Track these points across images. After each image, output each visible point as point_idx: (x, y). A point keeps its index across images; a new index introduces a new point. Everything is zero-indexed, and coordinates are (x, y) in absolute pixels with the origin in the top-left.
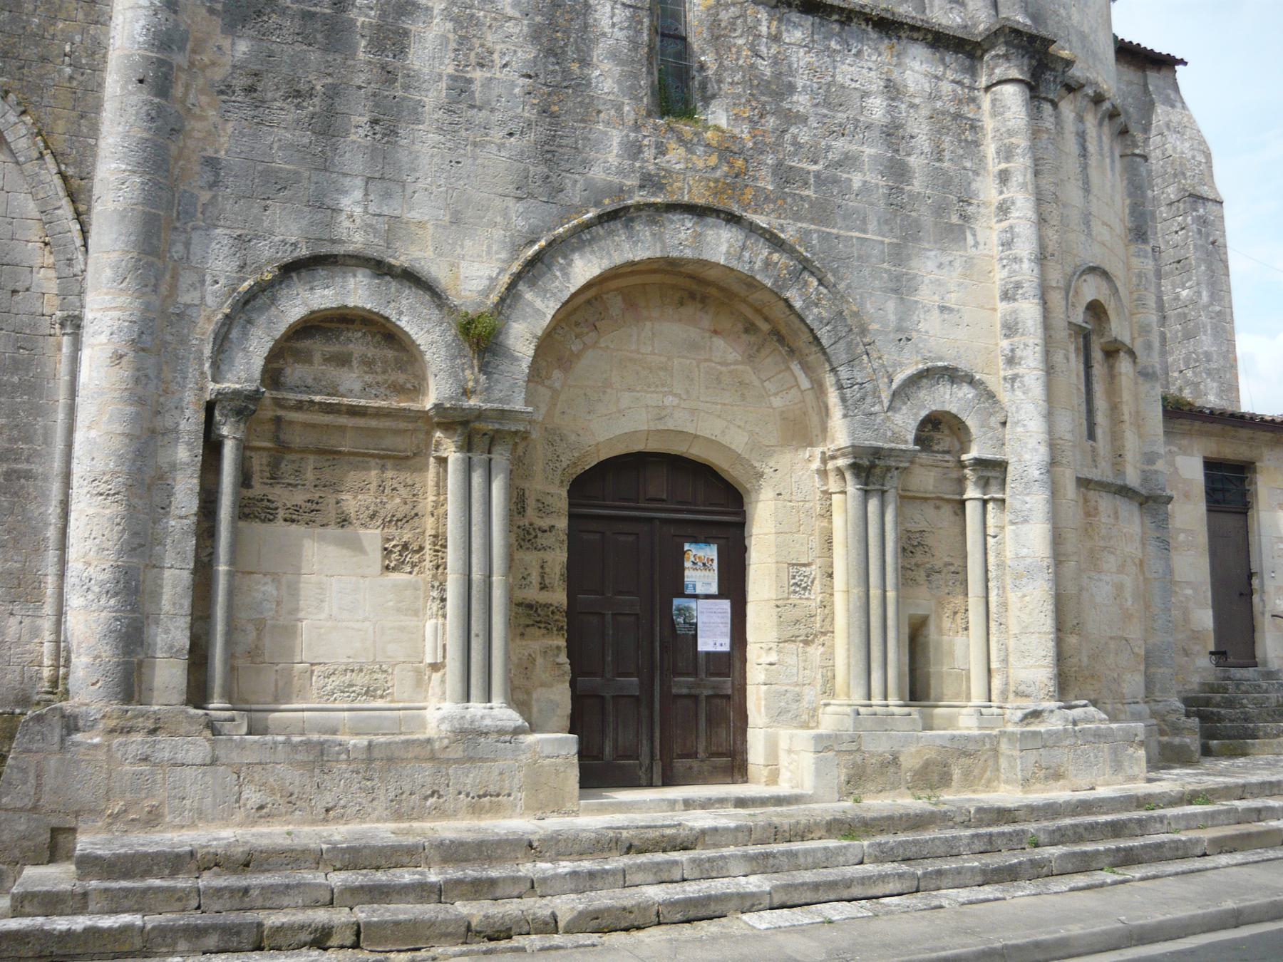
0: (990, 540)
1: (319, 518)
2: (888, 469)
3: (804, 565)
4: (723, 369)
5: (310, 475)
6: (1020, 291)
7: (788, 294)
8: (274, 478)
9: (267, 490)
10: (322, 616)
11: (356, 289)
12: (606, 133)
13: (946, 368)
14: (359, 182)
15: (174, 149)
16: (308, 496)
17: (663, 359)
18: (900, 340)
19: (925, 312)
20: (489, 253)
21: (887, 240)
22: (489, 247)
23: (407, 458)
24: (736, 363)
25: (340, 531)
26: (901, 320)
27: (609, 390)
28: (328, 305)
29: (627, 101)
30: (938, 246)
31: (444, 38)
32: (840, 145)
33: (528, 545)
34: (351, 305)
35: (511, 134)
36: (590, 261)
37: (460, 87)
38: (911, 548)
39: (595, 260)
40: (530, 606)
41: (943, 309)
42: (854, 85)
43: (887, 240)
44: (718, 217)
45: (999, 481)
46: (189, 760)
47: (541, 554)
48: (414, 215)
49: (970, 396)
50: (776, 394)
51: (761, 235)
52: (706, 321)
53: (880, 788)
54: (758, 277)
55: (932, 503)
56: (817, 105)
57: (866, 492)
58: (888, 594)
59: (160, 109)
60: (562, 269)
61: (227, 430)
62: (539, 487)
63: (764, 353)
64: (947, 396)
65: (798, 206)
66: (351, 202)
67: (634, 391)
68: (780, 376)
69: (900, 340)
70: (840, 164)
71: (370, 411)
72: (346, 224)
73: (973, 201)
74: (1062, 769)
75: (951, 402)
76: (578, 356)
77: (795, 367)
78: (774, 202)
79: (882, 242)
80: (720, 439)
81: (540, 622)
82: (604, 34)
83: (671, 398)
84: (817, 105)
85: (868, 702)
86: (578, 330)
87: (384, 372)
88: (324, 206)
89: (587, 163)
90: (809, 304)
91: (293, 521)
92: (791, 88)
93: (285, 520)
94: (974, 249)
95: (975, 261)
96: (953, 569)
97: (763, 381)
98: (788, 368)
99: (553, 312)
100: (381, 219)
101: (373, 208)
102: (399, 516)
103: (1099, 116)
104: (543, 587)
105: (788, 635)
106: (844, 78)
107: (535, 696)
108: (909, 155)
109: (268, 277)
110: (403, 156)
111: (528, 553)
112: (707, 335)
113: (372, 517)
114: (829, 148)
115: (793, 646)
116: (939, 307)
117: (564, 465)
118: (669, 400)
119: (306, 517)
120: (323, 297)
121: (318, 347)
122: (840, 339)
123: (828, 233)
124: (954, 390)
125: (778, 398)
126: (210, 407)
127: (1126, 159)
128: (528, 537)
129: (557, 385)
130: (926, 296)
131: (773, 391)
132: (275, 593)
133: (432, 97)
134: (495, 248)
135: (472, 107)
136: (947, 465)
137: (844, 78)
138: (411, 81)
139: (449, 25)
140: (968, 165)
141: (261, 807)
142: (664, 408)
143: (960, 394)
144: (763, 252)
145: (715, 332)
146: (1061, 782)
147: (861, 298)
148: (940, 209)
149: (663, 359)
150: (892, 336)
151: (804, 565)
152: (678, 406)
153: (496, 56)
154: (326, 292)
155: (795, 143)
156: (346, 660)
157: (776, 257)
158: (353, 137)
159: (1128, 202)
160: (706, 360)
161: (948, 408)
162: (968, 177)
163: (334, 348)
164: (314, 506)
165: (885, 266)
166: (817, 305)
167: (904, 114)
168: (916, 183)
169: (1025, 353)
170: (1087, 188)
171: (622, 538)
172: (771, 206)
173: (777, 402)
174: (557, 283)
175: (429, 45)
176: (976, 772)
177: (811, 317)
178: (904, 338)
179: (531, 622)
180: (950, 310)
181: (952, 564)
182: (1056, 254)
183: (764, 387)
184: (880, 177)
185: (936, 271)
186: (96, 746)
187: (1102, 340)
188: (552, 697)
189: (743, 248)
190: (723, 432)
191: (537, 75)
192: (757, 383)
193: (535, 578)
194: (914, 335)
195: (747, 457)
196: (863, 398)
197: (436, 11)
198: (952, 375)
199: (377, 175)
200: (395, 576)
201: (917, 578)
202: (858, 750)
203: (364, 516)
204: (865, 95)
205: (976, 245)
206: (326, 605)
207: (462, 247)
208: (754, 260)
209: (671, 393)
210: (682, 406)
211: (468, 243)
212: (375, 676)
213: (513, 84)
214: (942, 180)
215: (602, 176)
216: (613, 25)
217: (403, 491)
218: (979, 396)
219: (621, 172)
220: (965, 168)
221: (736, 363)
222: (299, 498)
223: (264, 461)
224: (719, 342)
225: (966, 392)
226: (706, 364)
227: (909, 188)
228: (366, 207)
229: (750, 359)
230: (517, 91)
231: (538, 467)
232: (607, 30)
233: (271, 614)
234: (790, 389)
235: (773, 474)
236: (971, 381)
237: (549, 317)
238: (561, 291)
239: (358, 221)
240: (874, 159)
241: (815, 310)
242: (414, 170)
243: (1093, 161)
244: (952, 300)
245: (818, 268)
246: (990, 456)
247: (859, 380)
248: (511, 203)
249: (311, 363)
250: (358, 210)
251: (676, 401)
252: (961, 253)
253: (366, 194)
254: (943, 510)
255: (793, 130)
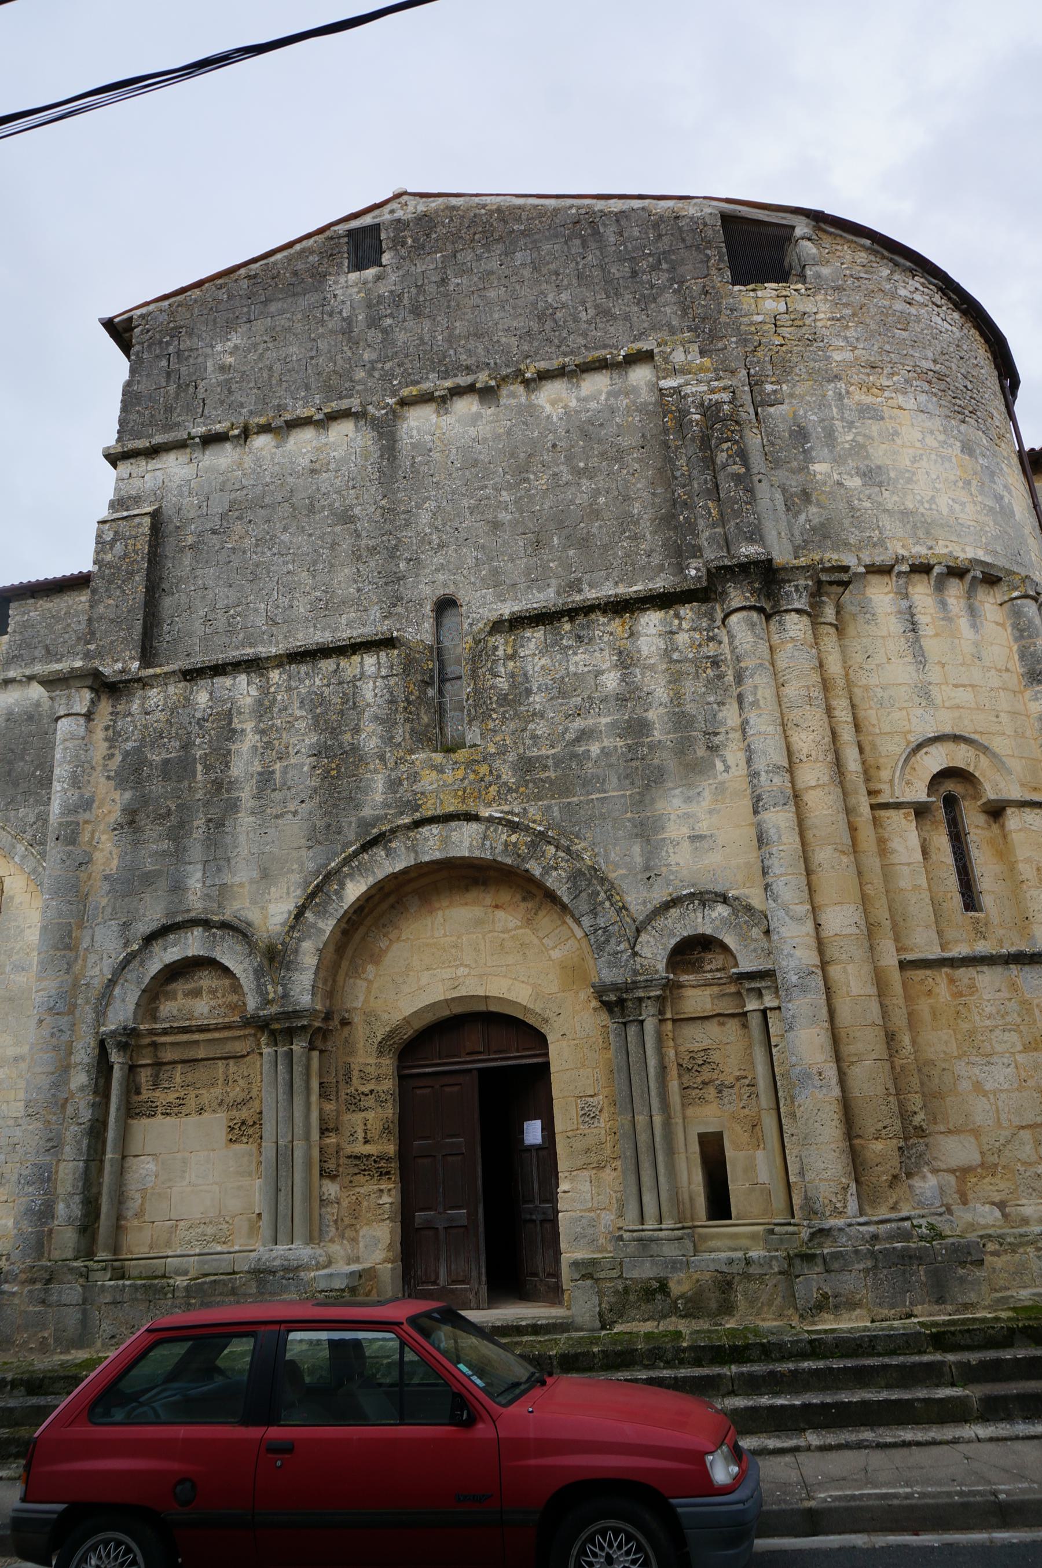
0: (774, 1050)
1: (185, 1111)
2: (640, 1000)
3: (591, 1096)
4: (506, 936)
5: (178, 1079)
6: (761, 804)
7: (528, 866)
8: (156, 1085)
9: (150, 1094)
10: (185, 1183)
11: (193, 944)
12: (373, 779)
13: (692, 894)
14: (200, 866)
15: (83, 876)
16: (177, 1095)
17: (454, 939)
18: (648, 879)
19: (674, 847)
20: (288, 893)
21: (628, 793)
22: (288, 888)
23: (243, 1056)
24: (516, 928)
25: (198, 1117)
26: (648, 859)
27: (411, 973)
28: (176, 958)
29: (388, 749)
30: (684, 782)
31: (255, 747)
32: (578, 724)
33: (353, 1107)
34: (190, 955)
35: (302, 802)
36: (358, 882)
37: (266, 779)
38: (696, 1067)
39: (362, 880)
40: (356, 1157)
41: (694, 838)
42: (586, 669)
43: (628, 793)
44: (460, 820)
45: (773, 990)
46: (68, 1302)
47: (363, 1114)
48: (237, 879)
49: (726, 914)
50: (554, 948)
51: (499, 823)
52: (488, 900)
53: (646, 1316)
54: (499, 859)
55: (715, 1020)
56: (552, 699)
57: (625, 1024)
58: (654, 1118)
59: (69, 854)
60: (336, 892)
61: (115, 1057)
62: (361, 1060)
63: (541, 914)
64: (700, 920)
65: (538, 788)
66: (195, 881)
67: (432, 969)
68: (557, 931)
69: (648, 879)
70: (578, 740)
71: (211, 1027)
72: (191, 897)
73: (720, 730)
74: (858, 1297)
75: (704, 924)
76: (386, 951)
77: (569, 920)
78: (516, 791)
79: (624, 796)
80: (506, 996)
81: (365, 1170)
82: (368, 705)
83: (462, 969)
84: (552, 699)
85: (641, 1227)
86: (384, 931)
87: (223, 997)
88: (178, 888)
89: (358, 807)
90: (547, 870)
91: (167, 1114)
92: (529, 692)
93: (163, 1114)
94: (725, 774)
95: (727, 785)
96: (747, 1082)
97: (541, 939)
98: (565, 922)
99: (331, 928)
100: (214, 889)
101: (208, 883)
102: (239, 1101)
103: (932, 583)
104: (366, 1142)
105: (579, 1163)
106: (577, 667)
107: (361, 1233)
108: (646, 711)
109: (136, 947)
110: (228, 839)
111: (354, 1115)
112: (490, 910)
113: (220, 1105)
114: (566, 729)
115: (586, 1173)
116: (689, 837)
117: (379, 1039)
118: (461, 971)
119: (176, 1110)
120: (171, 953)
121: (180, 987)
122: (580, 892)
123: (569, 803)
124: (706, 912)
125: (557, 950)
126: (102, 1045)
127: (1006, 606)
128: (354, 1101)
129: (371, 977)
130: (675, 830)
131: (551, 945)
132: (154, 1169)
133: (246, 794)
134: (292, 889)
135: (274, 790)
136: (721, 981)
137: (577, 667)
138: (232, 784)
139: (257, 737)
140: (712, 699)
141: (113, 1337)
142: (457, 978)
143: (714, 915)
144: (503, 835)
145: (497, 907)
146: (858, 1311)
147: (605, 851)
148: (683, 747)
149: (454, 939)
150: (639, 877)
151: (591, 1096)
152: (469, 974)
153: (290, 748)
154: (174, 949)
155: (534, 737)
156: (200, 1216)
157: (514, 838)
158: (195, 836)
159: (1015, 648)
160: (490, 931)
161: (700, 931)
162: (712, 710)
163: (190, 986)
164: (181, 1102)
165: (629, 815)
166: (556, 869)
167: (639, 677)
168: (656, 733)
169: (771, 862)
170: (920, 658)
171: (447, 1089)
172: (514, 795)
173: (556, 954)
174: (334, 905)
175: (245, 757)
176: (764, 1298)
177: (550, 880)
178: (650, 875)
179: (357, 1171)
180: (701, 837)
181: (746, 1077)
182: (813, 753)
183: (543, 944)
184: (618, 739)
185: (683, 806)
186: (14, 1294)
187: (979, 803)
188: (374, 1233)
189: (485, 837)
190: (509, 989)
191: (320, 752)
192: (536, 941)
193: (360, 1135)
194: (664, 869)
195: (532, 1007)
196: (607, 941)
197: (248, 730)
198: (704, 898)
199: (211, 858)
200: (236, 1147)
201: (706, 1096)
202: (620, 1277)
203: (215, 1104)
204: (599, 673)
205: (727, 769)
206: (187, 1175)
207: (269, 894)
208: (495, 845)
209: (461, 965)
210: (473, 973)
211: (273, 889)
212: (220, 1227)
213: (303, 765)
214: (681, 721)
215: (372, 812)
216: (376, 695)
217: (241, 1082)
218: (735, 912)
219: (386, 805)
220: (708, 703)
221: (516, 928)
222: (172, 1097)
223: (149, 1073)
224: (500, 914)
225: (721, 910)
226: (490, 935)
227: (649, 740)
228: (204, 882)
229: (529, 922)
230: (305, 769)
231: (360, 1045)
232: (371, 700)
233: (151, 1184)
234: (567, 940)
235: (555, 1019)
236: (725, 899)
237: (328, 932)
238: (336, 910)
239: (199, 893)
240: (613, 725)
241: (554, 873)
242: (236, 847)
243: (927, 630)
244: (703, 827)
245: (553, 838)
246: (754, 969)
247: (603, 925)
248: (304, 852)
249: (176, 999)
250: (199, 885)
251: (467, 970)
252: (711, 782)
253: (204, 873)
254: (728, 1026)
255: (531, 726)
